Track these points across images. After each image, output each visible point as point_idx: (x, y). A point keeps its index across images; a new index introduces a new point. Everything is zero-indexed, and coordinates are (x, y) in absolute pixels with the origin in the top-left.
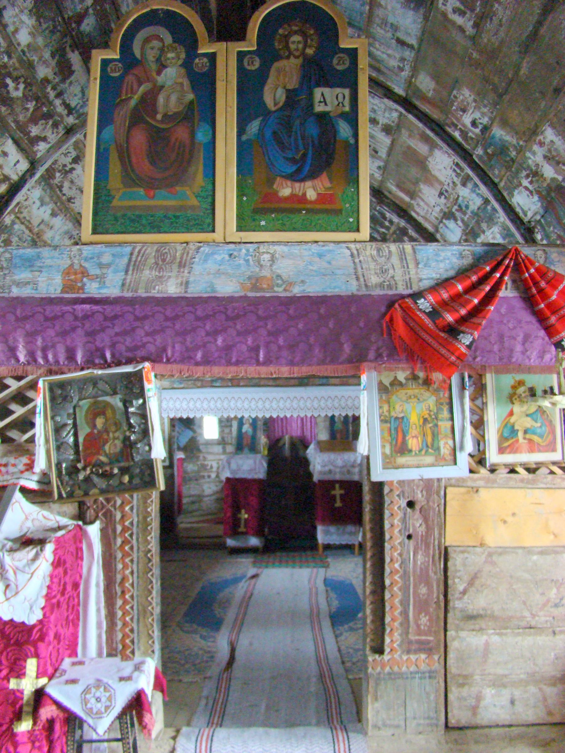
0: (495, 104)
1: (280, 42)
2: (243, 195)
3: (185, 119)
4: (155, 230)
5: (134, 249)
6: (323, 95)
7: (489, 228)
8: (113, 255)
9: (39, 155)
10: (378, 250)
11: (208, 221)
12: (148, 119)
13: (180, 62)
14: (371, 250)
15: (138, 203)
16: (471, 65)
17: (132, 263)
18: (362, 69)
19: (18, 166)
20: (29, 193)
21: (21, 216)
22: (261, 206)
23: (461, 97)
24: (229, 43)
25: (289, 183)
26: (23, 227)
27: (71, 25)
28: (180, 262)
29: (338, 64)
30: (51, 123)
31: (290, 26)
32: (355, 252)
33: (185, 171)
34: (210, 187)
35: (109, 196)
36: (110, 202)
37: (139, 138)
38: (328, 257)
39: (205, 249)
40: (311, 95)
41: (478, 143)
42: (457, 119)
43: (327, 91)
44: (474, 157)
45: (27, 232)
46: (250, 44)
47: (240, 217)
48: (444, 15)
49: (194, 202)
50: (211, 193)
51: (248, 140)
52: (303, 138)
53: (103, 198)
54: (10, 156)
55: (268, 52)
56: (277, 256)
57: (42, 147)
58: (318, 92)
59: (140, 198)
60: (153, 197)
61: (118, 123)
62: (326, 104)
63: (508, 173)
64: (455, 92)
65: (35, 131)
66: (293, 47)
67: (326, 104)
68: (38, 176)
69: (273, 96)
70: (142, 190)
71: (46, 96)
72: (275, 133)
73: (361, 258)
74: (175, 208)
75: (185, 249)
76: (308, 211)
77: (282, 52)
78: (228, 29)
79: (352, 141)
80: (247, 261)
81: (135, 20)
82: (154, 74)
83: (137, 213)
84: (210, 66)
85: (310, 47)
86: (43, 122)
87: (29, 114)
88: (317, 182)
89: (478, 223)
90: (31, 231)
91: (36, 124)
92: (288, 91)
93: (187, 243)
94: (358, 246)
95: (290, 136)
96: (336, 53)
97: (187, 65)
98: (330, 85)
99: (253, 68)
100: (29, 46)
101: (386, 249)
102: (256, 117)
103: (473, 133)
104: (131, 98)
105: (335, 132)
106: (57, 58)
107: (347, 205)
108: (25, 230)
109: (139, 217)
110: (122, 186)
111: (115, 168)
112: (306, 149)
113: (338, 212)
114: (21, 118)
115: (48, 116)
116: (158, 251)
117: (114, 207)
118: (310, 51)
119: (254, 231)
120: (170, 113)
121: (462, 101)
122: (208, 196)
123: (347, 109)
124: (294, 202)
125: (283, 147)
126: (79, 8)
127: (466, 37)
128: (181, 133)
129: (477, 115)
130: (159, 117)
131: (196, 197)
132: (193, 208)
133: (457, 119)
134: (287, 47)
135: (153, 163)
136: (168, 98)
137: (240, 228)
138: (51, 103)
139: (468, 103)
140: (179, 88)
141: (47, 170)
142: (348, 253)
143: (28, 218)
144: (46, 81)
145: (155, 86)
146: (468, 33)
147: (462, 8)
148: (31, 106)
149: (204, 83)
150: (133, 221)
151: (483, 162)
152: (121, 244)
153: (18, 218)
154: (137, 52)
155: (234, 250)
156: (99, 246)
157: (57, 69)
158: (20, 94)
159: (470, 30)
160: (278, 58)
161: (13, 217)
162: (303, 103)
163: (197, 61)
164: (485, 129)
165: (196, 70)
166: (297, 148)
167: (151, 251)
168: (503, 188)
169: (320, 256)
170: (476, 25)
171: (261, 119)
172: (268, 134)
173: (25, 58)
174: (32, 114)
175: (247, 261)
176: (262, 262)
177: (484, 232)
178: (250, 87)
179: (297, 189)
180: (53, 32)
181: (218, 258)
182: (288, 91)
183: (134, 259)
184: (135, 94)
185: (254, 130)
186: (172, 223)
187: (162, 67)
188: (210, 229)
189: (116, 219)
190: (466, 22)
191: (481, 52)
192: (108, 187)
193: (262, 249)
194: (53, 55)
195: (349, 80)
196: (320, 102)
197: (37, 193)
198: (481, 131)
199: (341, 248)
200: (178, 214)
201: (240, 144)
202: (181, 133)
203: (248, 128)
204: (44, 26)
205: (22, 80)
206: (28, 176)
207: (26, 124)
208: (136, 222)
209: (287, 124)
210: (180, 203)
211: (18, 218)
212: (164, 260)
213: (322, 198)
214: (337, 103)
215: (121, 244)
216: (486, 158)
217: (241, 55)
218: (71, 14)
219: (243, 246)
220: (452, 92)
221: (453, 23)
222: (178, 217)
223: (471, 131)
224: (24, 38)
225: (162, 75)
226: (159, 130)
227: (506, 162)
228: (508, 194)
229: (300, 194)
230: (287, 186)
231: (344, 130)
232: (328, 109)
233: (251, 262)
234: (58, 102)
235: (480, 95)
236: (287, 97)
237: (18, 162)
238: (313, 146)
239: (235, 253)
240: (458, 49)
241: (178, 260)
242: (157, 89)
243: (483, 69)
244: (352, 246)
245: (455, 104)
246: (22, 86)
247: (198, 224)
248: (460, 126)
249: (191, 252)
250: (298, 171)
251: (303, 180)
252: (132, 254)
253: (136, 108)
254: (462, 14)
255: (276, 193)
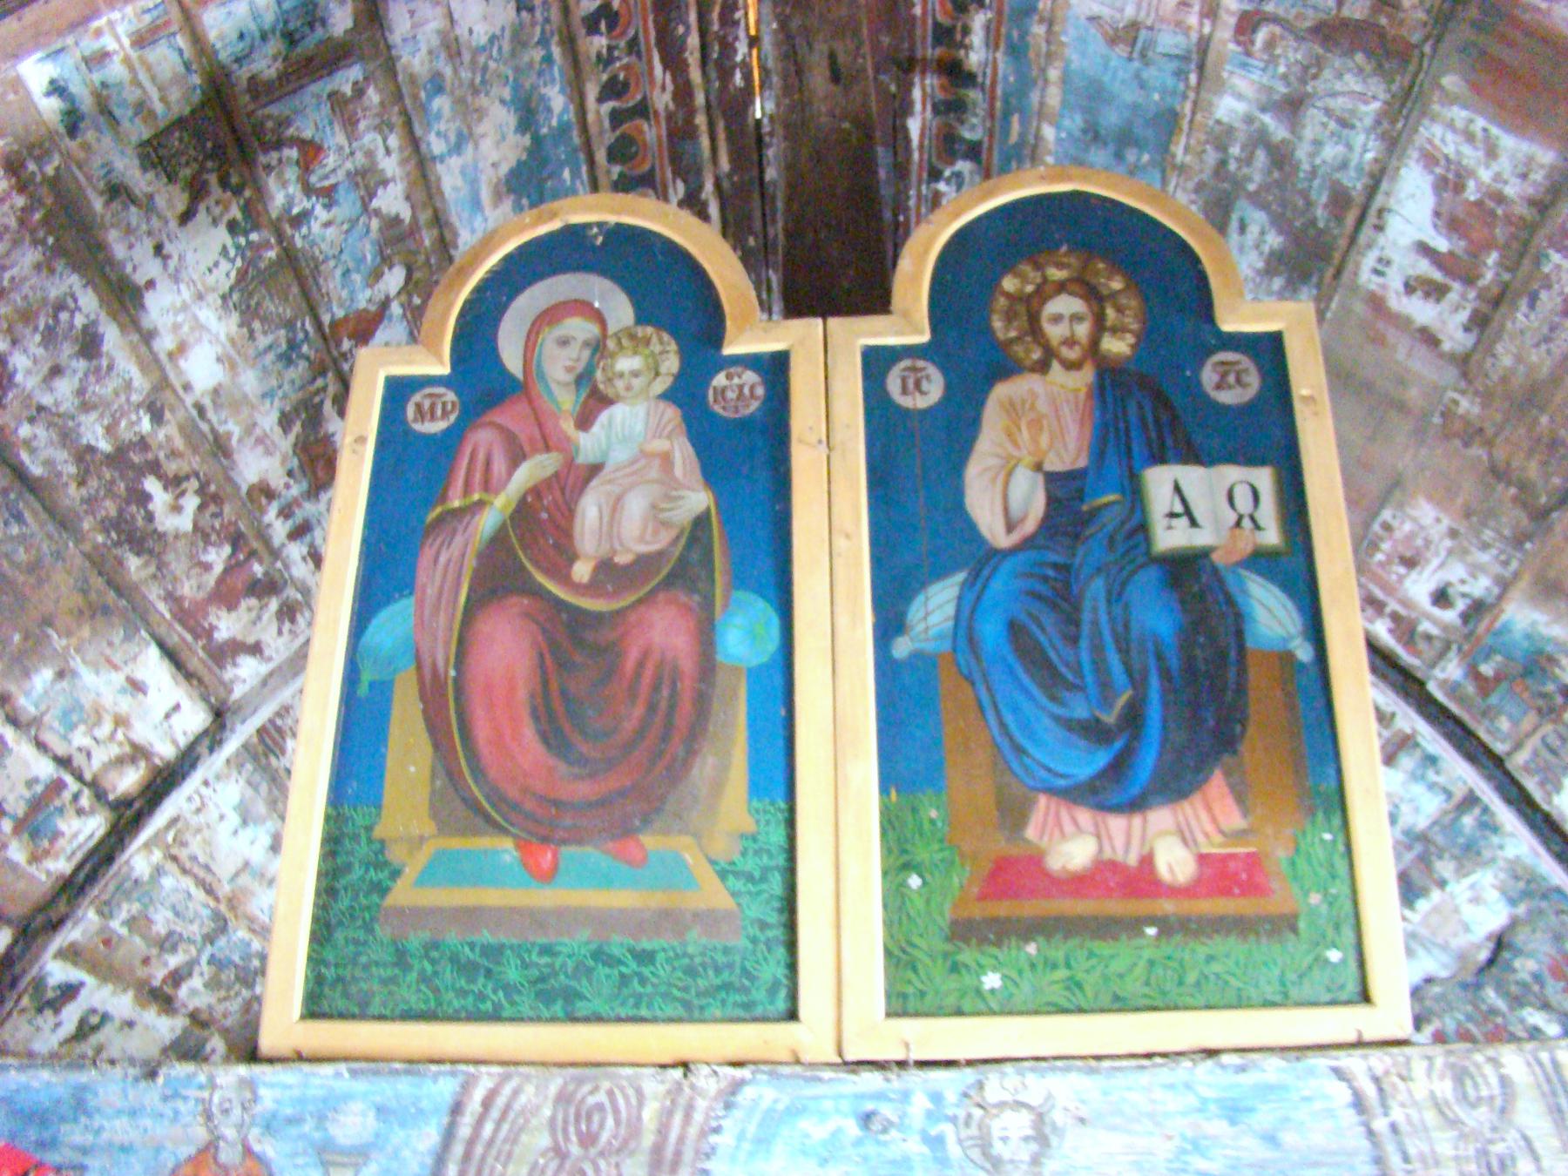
0: (1518, 541)
1: (1010, 316)
2: (907, 867)
3: (669, 582)
4: (558, 1008)
5: (467, 1086)
6: (1177, 489)
7: (1462, 872)
8: (382, 1111)
9: (238, 692)
10: (1460, 1076)
11: (773, 969)
12: (541, 578)
13: (661, 385)
14: (1427, 1076)
15: (491, 897)
16: (1447, 436)
17: (458, 1149)
18: (1310, 400)
19: (175, 718)
20: (204, 790)
21: (183, 854)
22: (978, 911)
23: (1407, 527)
24: (834, 323)
25: (1084, 816)
26: (188, 883)
27: (339, 344)
28: (657, 1150)
29: (1218, 387)
30: (274, 604)
31: (1038, 267)
32: (1370, 1090)
33: (677, 772)
34: (778, 836)
35: (380, 865)
36: (382, 890)
37: (507, 648)
38: (1264, 1117)
39: (760, 1092)
40: (1135, 494)
41: (1447, 647)
42: (1385, 586)
43: (1192, 477)
44: (1432, 687)
45: (199, 895)
46: (907, 322)
47: (899, 958)
48: (1377, 303)
49: (714, 895)
50: (781, 860)
51: (917, 656)
52: (1124, 650)
53: (358, 872)
54: (151, 692)
55: (973, 347)
56: (1057, 1116)
57: (247, 671)
58: (1160, 482)
59: (496, 879)
60: (546, 876)
61: (431, 591)
62: (1194, 523)
63: (1548, 728)
64: (1386, 515)
65: (227, 625)
66: (1055, 332)
67: (1194, 523)
68: (232, 745)
69: (1001, 493)
70: (508, 844)
71: (263, 535)
72: (1015, 630)
73: (1397, 1114)
74: (636, 923)
75: (678, 1087)
76: (1167, 927)
77: (1019, 350)
78: (831, 267)
79: (1304, 653)
80: (936, 1142)
81: (508, 258)
82: (568, 426)
83: (486, 937)
84: (768, 398)
85: (1116, 331)
86: (253, 602)
87: (211, 579)
88: (1191, 811)
89: (1424, 861)
90: (210, 891)
91: (232, 606)
92: (1052, 479)
93: (685, 1065)
94: (1379, 1061)
95: (1074, 640)
96: (1211, 352)
97: (686, 392)
98: (1193, 455)
99: (922, 403)
100: (216, 392)
101: (1488, 1069)
102: (941, 573)
103: (1435, 622)
104: (481, 504)
105: (1238, 620)
106: (297, 428)
107: (1315, 898)
108: (193, 889)
109: (494, 953)
110: (429, 827)
111: (408, 757)
112: (1138, 681)
113: (1285, 924)
114: (187, 589)
115: (267, 587)
116: (563, 1098)
117: (399, 912)
118: (1117, 346)
119: (959, 1013)
120: (622, 559)
121: (1410, 537)
122: (765, 870)
123: (1271, 536)
124: (1108, 892)
125: (1052, 679)
126: (364, 299)
127: (1441, 355)
128: (665, 631)
129: (1455, 572)
130: (582, 571)
131: (722, 875)
132: (709, 920)
133: (1385, 586)
134: (1034, 329)
135: (553, 737)
136: (617, 504)
137: (900, 1006)
138: (275, 554)
139: (1428, 543)
140: (654, 473)
141: (262, 732)
142: (1343, 1094)
143: (202, 859)
144: (265, 491)
145: (570, 463)
146: (1446, 346)
147: (1437, 276)
148: (218, 557)
149: (749, 452)
150: (467, 969)
151: (1462, 700)
152: (415, 1063)
153: (175, 859)
154: (511, 357)
155: (880, 1096)
156: (327, 1070)
157: (295, 462)
158: (184, 522)
159: (1455, 337)
160: (1005, 368)
161: (157, 855)
162: (1110, 520)
163: (720, 380)
164: (1477, 608)
165: (718, 409)
166: (1105, 685)
167: (536, 1096)
168: (1526, 768)
169: (1234, 1111)
170: (1479, 322)
171: (960, 577)
172: (992, 631)
173: (205, 427)
174: (220, 581)
175: (936, 1142)
176: (998, 1148)
177: (1442, 884)
178: (912, 466)
179: (1119, 841)
180: (287, 359)
181: (815, 1129)
182: (1052, 479)
183: (464, 1131)
184: (497, 492)
185: (934, 619)
186: (624, 980)
187: (595, 401)
188: (781, 1004)
189: (401, 959)
190: (1448, 319)
191: (1486, 397)
192: (378, 832)
193: (998, 1086)
194: (285, 422)
195: (1265, 434)
196: (1172, 515)
197: (230, 792)
198: (1465, 617)
199: (1311, 1072)
200: (646, 944)
201: (886, 668)
202: (665, 631)
203: (915, 612)
204: (263, 341)
205: (194, 484)
206: (203, 749)
207: (201, 607)
208: (478, 976)
209: (1060, 594)
210: (657, 900)
211: (175, 859)
212: (588, 1140)
213: (1220, 875)
214: (1232, 518)
215: (415, 1063)
216: (1470, 689)
217: (876, 362)
218: (340, 314)
219: (915, 1077)
220: (1377, 514)
221: (1402, 322)
222: (645, 957)
223: (1429, 617)
224: (202, 370)
225: (596, 428)
226: (580, 619)
227: (1543, 696)
228: (1542, 784)
229: (1132, 860)
230: (1079, 829)
231: (1269, 614)
232: (1201, 538)
233: (954, 1150)
234: (296, 551)
235: (1475, 515)
236: (1051, 500)
237: (177, 707)
238: (1165, 674)
239: (887, 1110)
240: (1413, 394)
241: (648, 1140)
242: (578, 476)
243: (1489, 444)
244: (1353, 1062)
245: (1386, 546)
246: (191, 503)
247: (727, 987)
248: (1393, 606)
249: (701, 1104)
250: (1117, 769)
251: (1136, 805)
252: (457, 1109)
253: (498, 540)
254: (1435, 291)
255: (1035, 861)
